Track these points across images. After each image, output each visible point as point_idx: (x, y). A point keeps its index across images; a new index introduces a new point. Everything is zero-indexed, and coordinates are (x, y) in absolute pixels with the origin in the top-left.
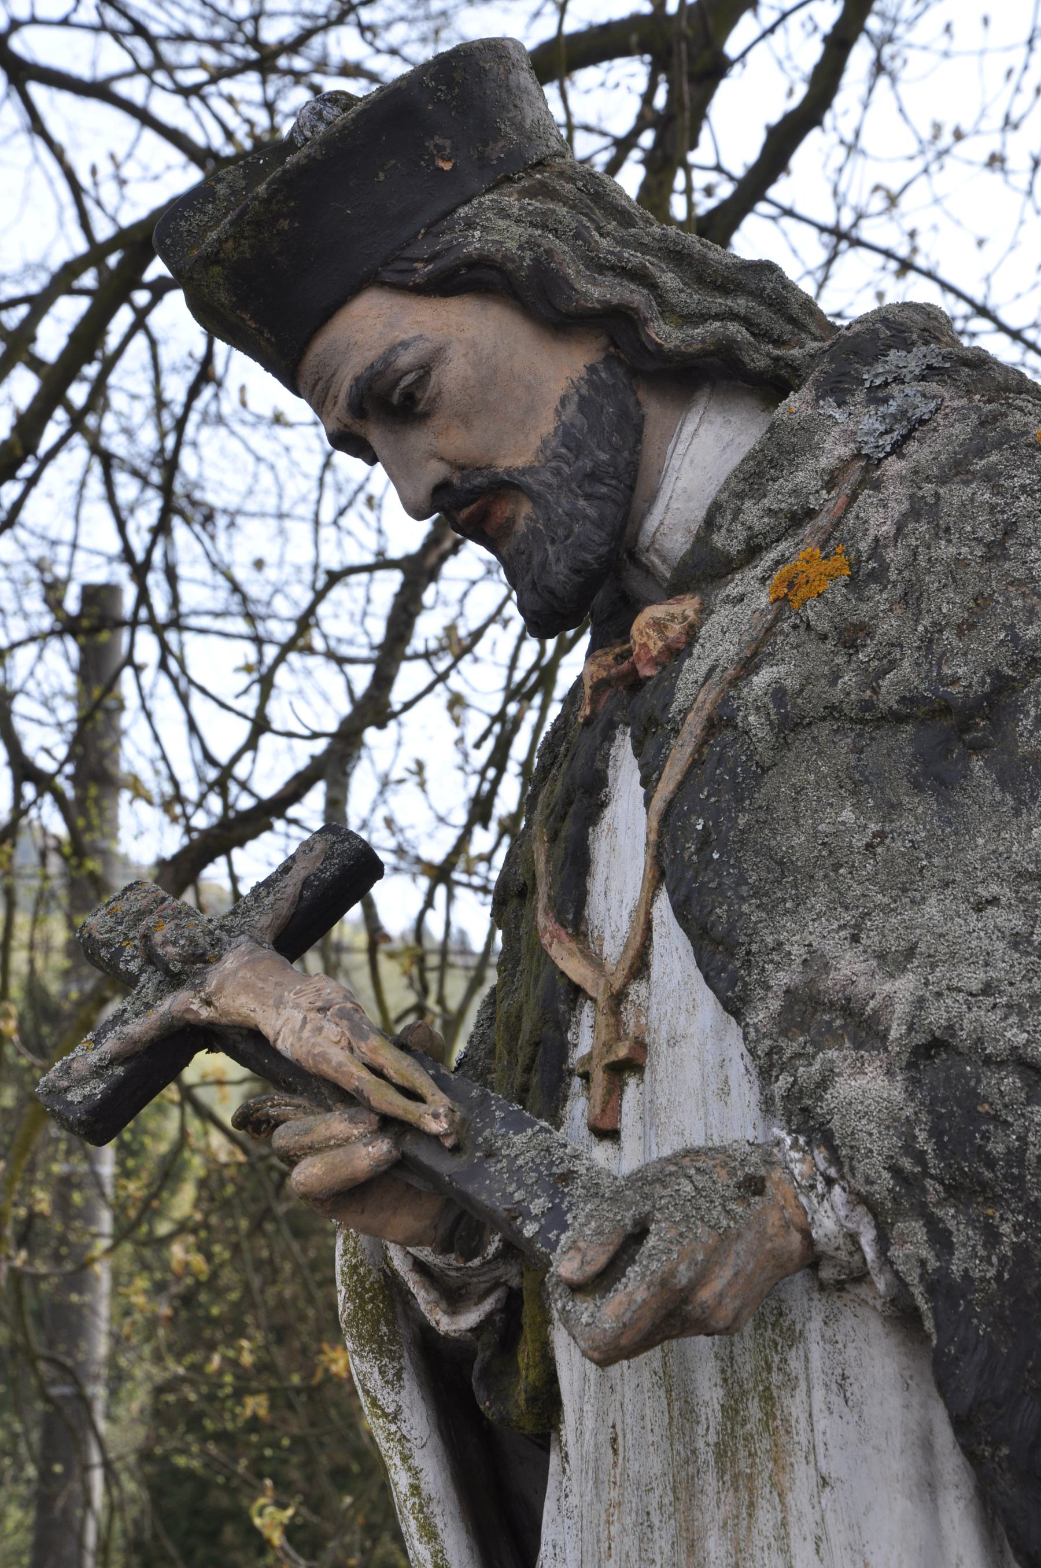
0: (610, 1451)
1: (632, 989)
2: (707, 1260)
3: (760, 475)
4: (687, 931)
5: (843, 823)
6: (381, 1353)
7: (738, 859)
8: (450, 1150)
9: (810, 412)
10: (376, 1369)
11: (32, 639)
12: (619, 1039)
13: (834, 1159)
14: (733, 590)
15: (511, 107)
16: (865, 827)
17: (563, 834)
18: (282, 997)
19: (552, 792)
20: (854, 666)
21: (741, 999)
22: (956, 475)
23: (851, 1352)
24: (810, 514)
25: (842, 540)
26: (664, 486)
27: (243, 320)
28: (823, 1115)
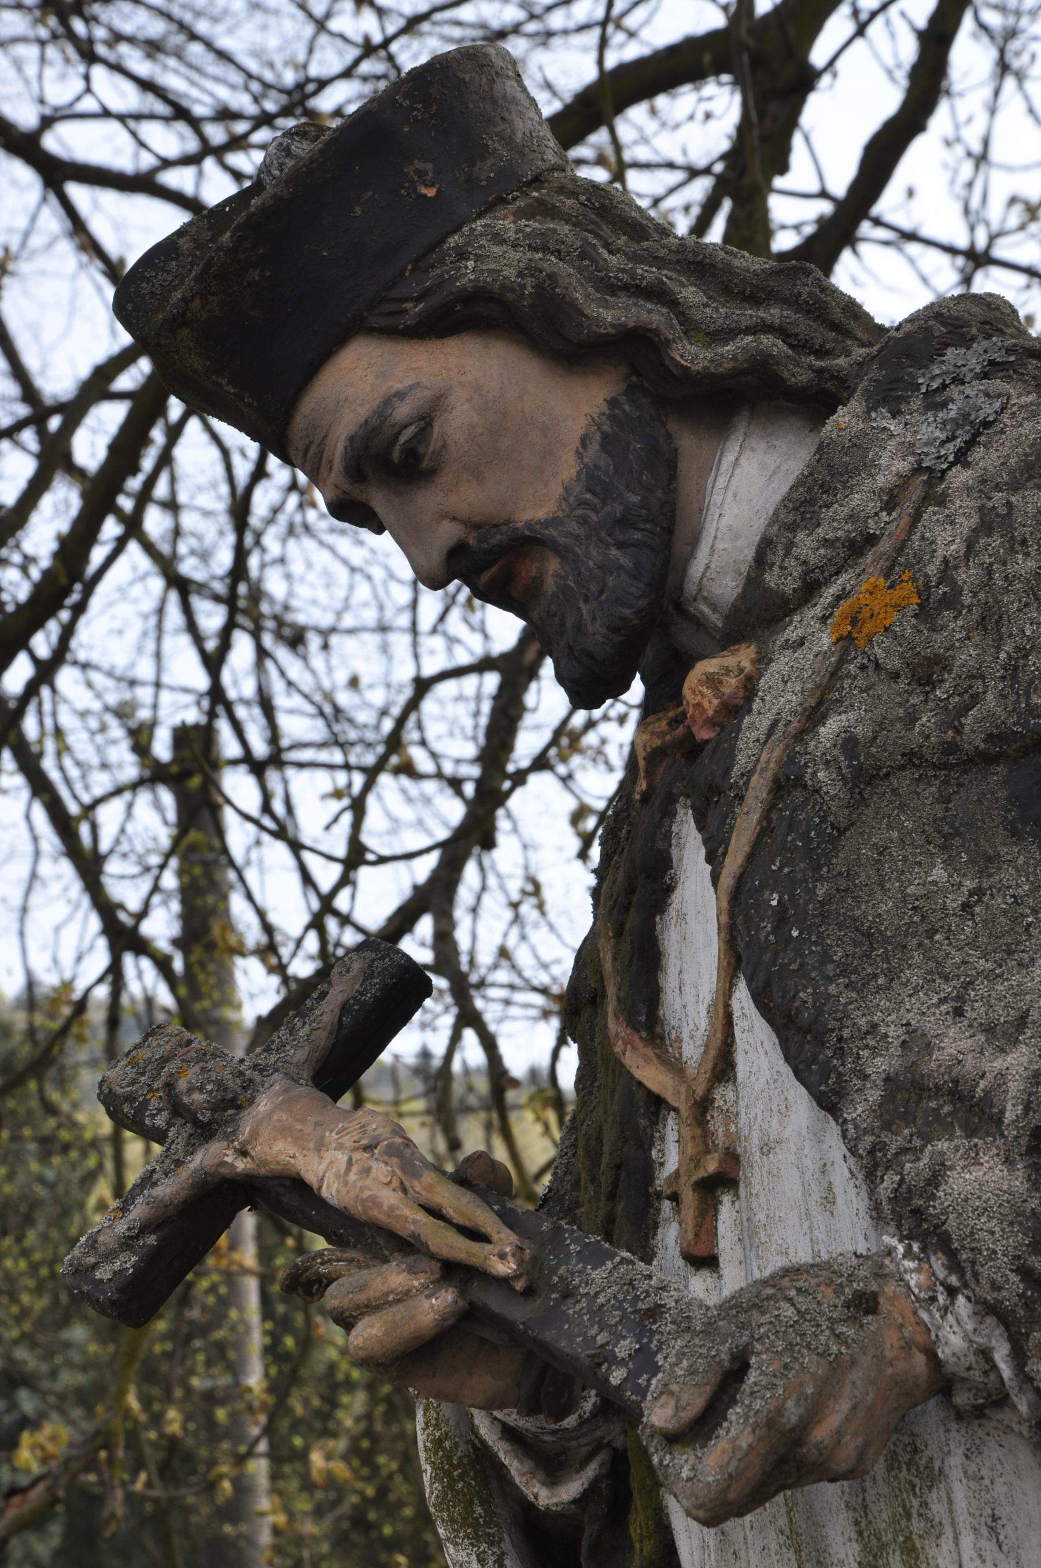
1: (718, 1093)
2: (818, 1393)
3: (811, 502)
5: (934, 883)
7: (820, 935)
8: (522, 1294)
9: (861, 426)
10: (474, 1557)
11: (118, 791)
12: (708, 1152)
13: (954, 1265)
14: (791, 633)
15: (498, 120)
16: (960, 885)
17: (628, 926)
18: (323, 1137)
19: (615, 881)
20: (931, 705)
21: (837, 1093)
22: (1028, 480)
23: (1000, 1489)
24: (871, 540)
25: (908, 566)
26: (706, 525)
27: (220, 385)
28: (937, 1216)
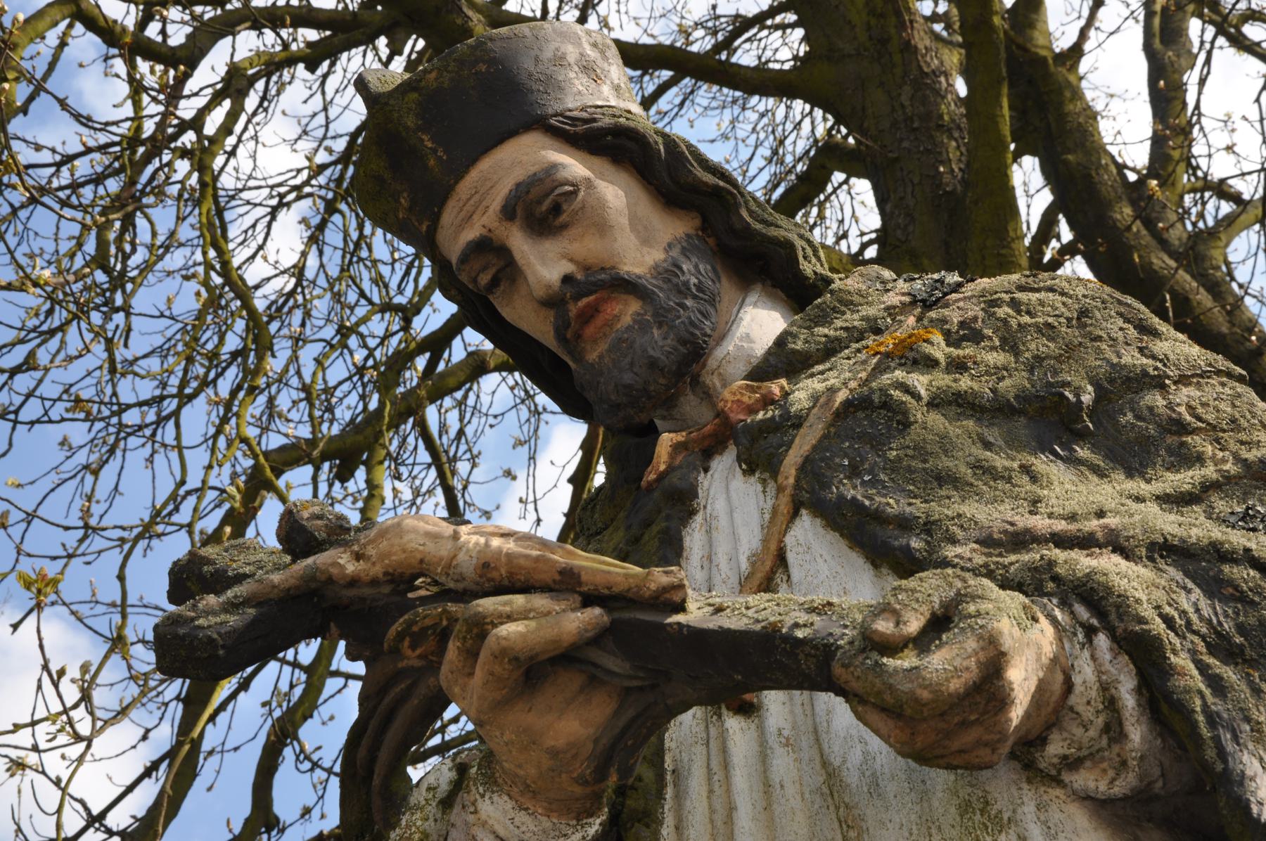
27: (423, 140)
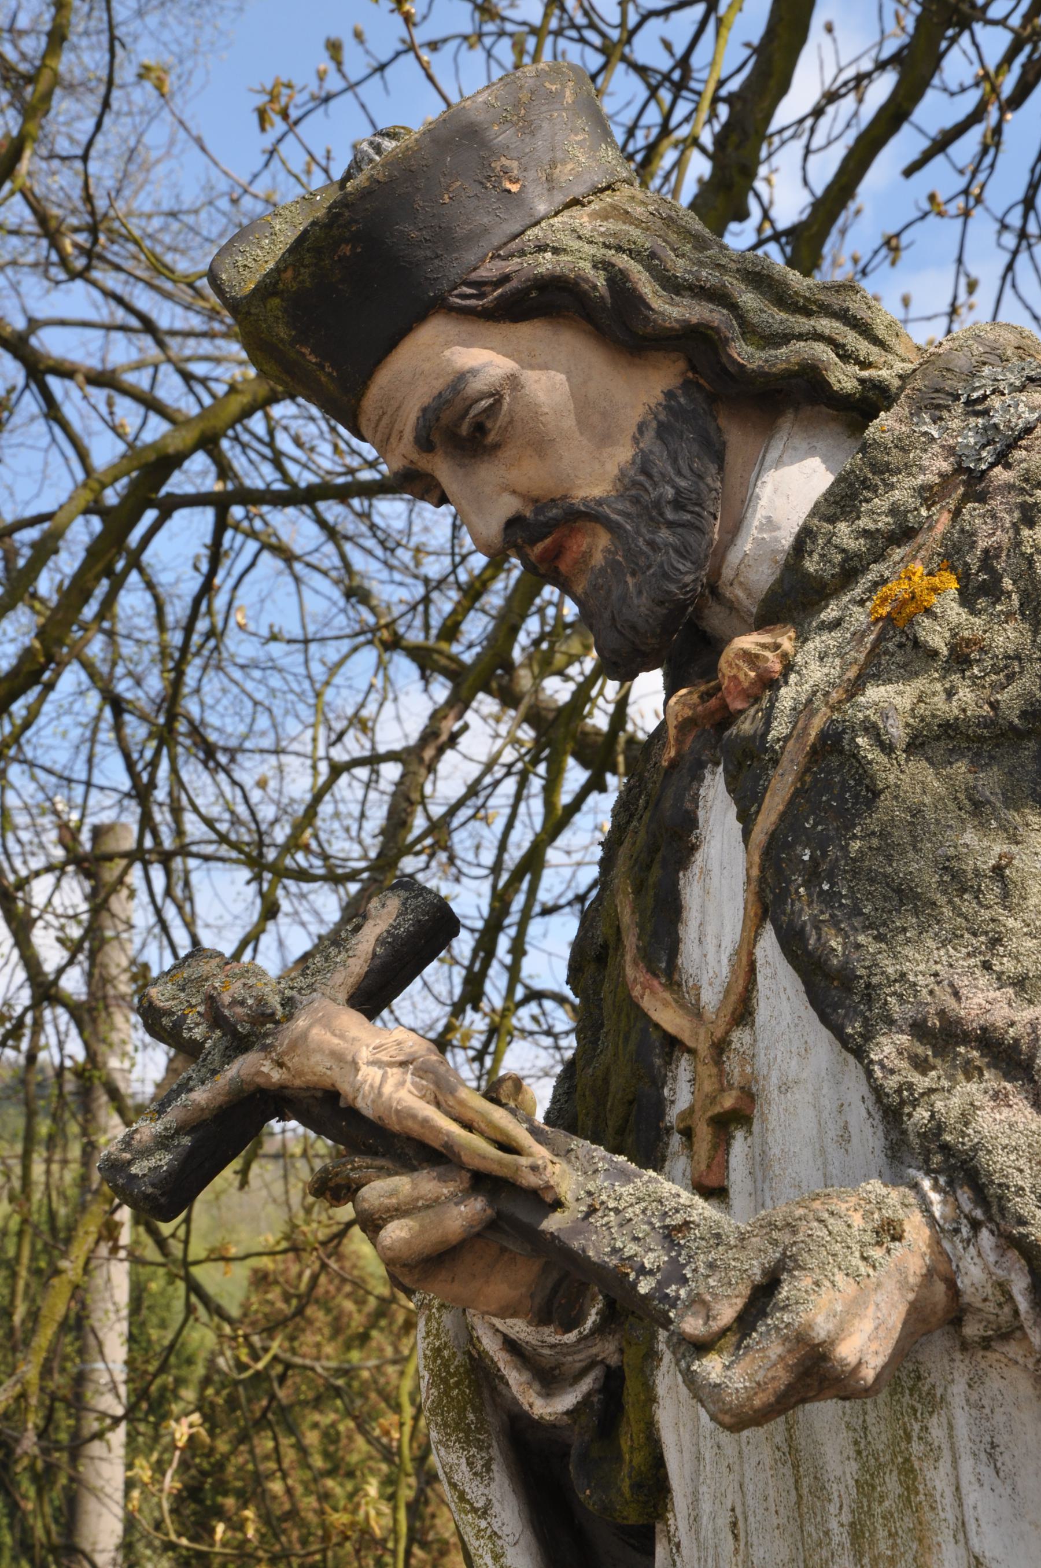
0: (730, 1537)
4: (797, 968)
6: (468, 1442)
10: (463, 1460)
12: (722, 1090)
14: (830, 613)
17: (651, 880)
23: (999, 1418)
27: (303, 355)
28: (966, 1152)
